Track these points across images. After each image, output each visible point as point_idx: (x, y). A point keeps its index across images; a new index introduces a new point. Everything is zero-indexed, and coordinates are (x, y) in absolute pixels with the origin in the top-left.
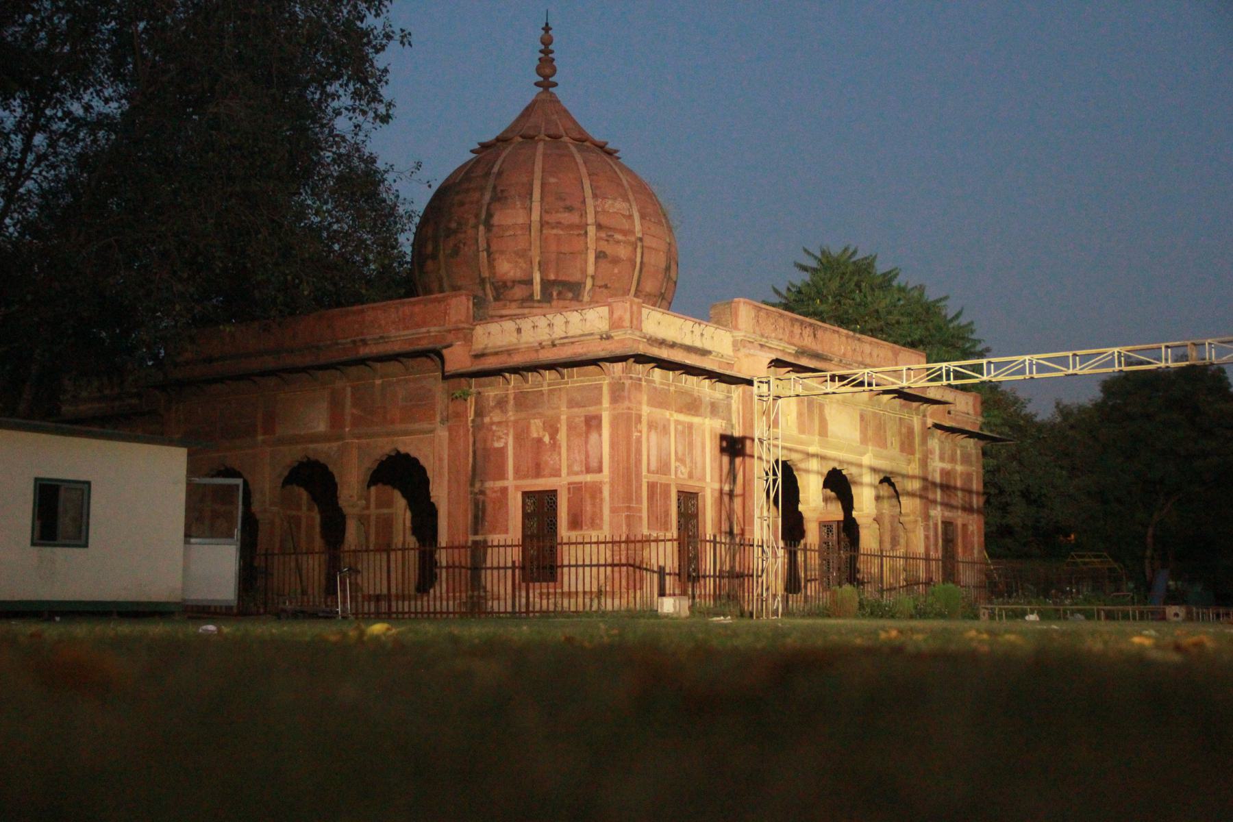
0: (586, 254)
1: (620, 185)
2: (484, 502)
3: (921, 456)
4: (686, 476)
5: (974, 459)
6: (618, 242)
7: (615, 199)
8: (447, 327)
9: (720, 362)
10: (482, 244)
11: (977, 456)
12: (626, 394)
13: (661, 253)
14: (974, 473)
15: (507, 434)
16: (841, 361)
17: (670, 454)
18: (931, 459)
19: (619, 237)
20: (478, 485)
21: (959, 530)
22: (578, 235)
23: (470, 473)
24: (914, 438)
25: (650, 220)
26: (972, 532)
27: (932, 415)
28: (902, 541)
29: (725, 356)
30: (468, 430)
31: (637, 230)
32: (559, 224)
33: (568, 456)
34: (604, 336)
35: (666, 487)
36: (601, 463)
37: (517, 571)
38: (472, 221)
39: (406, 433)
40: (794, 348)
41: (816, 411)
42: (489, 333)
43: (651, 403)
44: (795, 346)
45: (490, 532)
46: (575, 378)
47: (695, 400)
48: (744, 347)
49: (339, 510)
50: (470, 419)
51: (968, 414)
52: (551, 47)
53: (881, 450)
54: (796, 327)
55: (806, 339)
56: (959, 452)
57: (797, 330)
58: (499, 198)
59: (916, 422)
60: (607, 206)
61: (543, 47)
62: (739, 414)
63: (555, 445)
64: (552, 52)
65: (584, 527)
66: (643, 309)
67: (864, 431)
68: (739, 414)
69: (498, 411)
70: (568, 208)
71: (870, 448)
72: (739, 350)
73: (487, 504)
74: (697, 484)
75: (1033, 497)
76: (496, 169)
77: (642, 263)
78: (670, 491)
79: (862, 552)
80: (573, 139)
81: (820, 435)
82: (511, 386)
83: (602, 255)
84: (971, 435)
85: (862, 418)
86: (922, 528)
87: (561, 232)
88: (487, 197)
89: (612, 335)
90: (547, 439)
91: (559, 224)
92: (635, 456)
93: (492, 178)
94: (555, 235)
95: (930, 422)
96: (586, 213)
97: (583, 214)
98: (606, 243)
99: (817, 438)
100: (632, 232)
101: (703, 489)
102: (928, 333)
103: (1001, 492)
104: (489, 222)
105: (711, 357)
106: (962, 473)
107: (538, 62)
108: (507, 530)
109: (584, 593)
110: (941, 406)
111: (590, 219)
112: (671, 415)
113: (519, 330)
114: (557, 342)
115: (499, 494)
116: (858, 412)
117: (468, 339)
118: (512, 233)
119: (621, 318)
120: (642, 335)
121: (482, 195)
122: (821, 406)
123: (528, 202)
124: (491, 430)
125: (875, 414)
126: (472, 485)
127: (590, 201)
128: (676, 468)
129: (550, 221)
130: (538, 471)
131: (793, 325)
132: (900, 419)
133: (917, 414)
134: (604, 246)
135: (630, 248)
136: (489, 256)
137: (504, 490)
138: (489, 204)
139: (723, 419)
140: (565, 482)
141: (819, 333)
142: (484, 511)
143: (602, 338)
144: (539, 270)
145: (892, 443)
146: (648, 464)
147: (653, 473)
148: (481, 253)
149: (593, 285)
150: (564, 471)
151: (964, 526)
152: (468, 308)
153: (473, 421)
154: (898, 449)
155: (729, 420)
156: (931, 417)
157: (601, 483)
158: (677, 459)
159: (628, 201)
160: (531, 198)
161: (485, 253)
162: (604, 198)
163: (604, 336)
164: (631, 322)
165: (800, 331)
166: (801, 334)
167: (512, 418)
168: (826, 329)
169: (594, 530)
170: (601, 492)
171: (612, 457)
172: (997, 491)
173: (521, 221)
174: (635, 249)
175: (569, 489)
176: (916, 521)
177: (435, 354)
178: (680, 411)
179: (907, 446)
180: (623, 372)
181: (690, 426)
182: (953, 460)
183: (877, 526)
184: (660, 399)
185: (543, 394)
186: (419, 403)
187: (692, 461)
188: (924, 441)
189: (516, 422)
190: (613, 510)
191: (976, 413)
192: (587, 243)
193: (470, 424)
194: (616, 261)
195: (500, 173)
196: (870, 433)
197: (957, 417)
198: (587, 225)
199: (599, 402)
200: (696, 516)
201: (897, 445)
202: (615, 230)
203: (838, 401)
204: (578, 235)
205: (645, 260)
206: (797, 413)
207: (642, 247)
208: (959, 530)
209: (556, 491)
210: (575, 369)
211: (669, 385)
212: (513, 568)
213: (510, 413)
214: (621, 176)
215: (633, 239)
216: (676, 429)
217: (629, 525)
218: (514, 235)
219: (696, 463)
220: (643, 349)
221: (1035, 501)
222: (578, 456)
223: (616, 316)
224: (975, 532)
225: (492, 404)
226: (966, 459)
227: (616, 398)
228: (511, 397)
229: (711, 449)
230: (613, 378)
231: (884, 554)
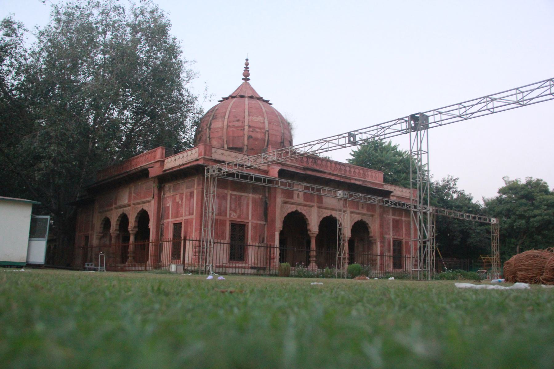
0: (244, 137)
4: (236, 217)
6: (257, 132)
17: (226, 208)
19: (257, 130)
22: (241, 130)
52: (248, 66)
55: (310, 163)
60: (253, 119)
61: (245, 66)
63: (182, 204)
64: (248, 68)
79: (312, 249)
87: (234, 129)
90: (180, 202)
98: (252, 133)
99: (315, 204)
106: (405, 221)
107: (243, 71)
118: (217, 130)
121: (210, 118)
123: (223, 119)
128: (230, 213)
130: (177, 216)
135: (263, 134)
136: (210, 139)
137: (168, 223)
138: (211, 121)
142: (163, 231)
144: (227, 144)
149: (247, 149)
150: (184, 215)
151: (407, 243)
162: (252, 116)
167: (172, 195)
173: (220, 126)
174: (265, 134)
181: (240, 197)
192: (244, 133)
198: (244, 126)
207: (269, 134)
215: (264, 131)
231: (407, 256)
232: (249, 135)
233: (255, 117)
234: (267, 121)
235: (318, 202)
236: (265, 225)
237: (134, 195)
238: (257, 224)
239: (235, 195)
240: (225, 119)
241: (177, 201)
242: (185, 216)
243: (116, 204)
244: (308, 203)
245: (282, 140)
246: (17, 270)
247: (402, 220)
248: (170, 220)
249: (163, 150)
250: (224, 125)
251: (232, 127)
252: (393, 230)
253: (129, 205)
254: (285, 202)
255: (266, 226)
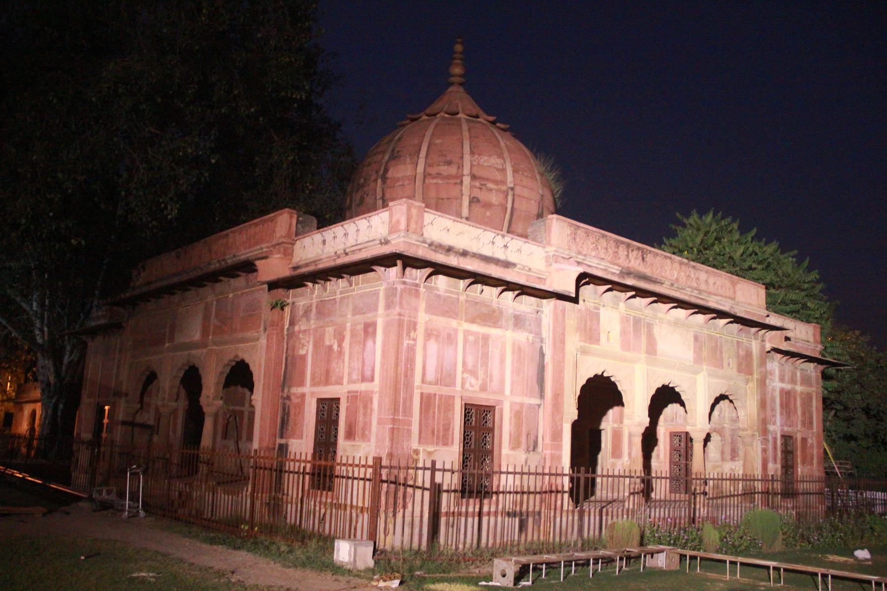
0: (461, 199)
1: (498, 145)
2: (289, 407)
3: (759, 377)
4: (477, 388)
5: (814, 380)
6: (491, 190)
7: (490, 156)
8: (274, 242)
9: (528, 275)
10: (379, 195)
11: (817, 379)
12: (397, 299)
13: (533, 202)
14: (814, 394)
15: (308, 342)
16: (672, 285)
17: (455, 364)
18: (771, 379)
19: (490, 185)
20: (286, 390)
21: (799, 442)
22: (456, 183)
23: (282, 378)
24: (752, 359)
25: (523, 174)
26: (812, 446)
27: (772, 340)
28: (741, 453)
29: (532, 270)
30: (284, 339)
31: (508, 180)
32: (439, 175)
33: (349, 363)
34: (383, 241)
35: (448, 402)
36: (373, 370)
37: (307, 477)
38: (373, 177)
39: (244, 340)
40: (617, 267)
41: (644, 331)
42: (304, 247)
43: (430, 310)
44: (619, 266)
45: (290, 438)
46: (360, 286)
47: (494, 311)
48: (556, 262)
49: (201, 408)
50: (286, 327)
51: (808, 342)
53: (717, 370)
54: (621, 249)
55: (633, 261)
56: (798, 374)
57: (622, 251)
58: (395, 157)
59: (755, 347)
60: (482, 160)
62: (549, 328)
63: (341, 353)
65: (357, 438)
66: (426, 215)
67: (698, 350)
68: (549, 328)
69: (304, 320)
70: (447, 162)
71: (705, 367)
72: (551, 265)
73: (291, 409)
74: (492, 397)
75: (872, 413)
76: (397, 138)
77: (512, 208)
78: (454, 404)
80: (469, 116)
81: (648, 352)
82: (314, 296)
83: (475, 200)
84: (810, 359)
85: (696, 338)
86: (759, 442)
87: (440, 182)
88: (387, 157)
89: (389, 239)
90: (335, 347)
91: (439, 175)
92: (406, 365)
93: (393, 144)
94: (435, 184)
95: (768, 347)
96: (463, 166)
97: (460, 167)
98: (479, 190)
99: (643, 356)
100: (504, 182)
101: (500, 402)
102: (778, 279)
103: (846, 409)
104: (385, 175)
105: (516, 269)
106: (802, 393)
108: (302, 435)
109: (352, 506)
110: (779, 332)
111: (466, 171)
112: (459, 324)
113: (324, 242)
114: (347, 251)
115: (299, 400)
116: (692, 334)
117: (288, 253)
118: (401, 183)
119: (398, 222)
120: (421, 239)
122: (650, 327)
123: (416, 158)
124: (299, 338)
125: (710, 337)
126: (283, 390)
127: (467, 157)
129: (431, 173)
130: (327, 382)
131: (618, 247)
132: (738, 342)
133: (755, 339)
134: (477, 193)
135: (502, 196)
137: (303, 396)
138: (387, 162)
139: (531, 332)
140: (346, 391)
141: (649, 258)
142: (288, 413)
143: (381, 243)
145: (729, 364)
146: (424, 375)
147: (430, 383)
148: (378, 201)
150: (345, 380)
151: (804, 440)
152: (290, 225)
153: (288, 329)
154: (735, 370)
155: (538, 334)
156: (769, 342)
157: (372, 392)
158: (465, 369)
159: (503, 158)
160: (418, 156)
161: (381, 202)
162: (480, 155)
163: (383, 241)
164: (408, 225)
165: (626, 253)
166: (627, 256)
167: (313, 326)
168: (657, 254)
169: (363, 441)
170: (372, 402)
171: (383, 365)
172: (842, 408)
175: (348, 397)
176: (753, 435)
177: (248, 267)
178: (473, 321)
179: (745, 365)
180: (397, 278)
181: (486, 338)
182: (793, 381)
183: (720, 438)
184: (445, 307)
185: (336, 302)
186: (252, 313)
187: (486, 372)
188: (763, 363)
189: (316, 330)
190: (380, 422)
191: (816, 342)
192: (461, 191)
193: (285, 333)
194: (488, 205)
195: (400, 139)
196: (705, 353)
197: (798, 344)
199: (376, 309)
200: (492, 430)
201: (733, 363)
202: (487, 179)
203: (669, 321)
204: (456, 183)
205: (516, 206)
206: (621, 331)
207: (514, 195)
208: (799, 442)
209: (339, 399)
210: (361, 276)
211: (458, 294)
212: (304, 473)
213: (312, 322)
214: (499, 138)
215: (504, 188)
216: (465, 340)
217: (392, 440)
218: (403, 185)
219: (491, 376)
220: (422, 252)
221: (875, 416)
222: (357, 365)
223: (394, 220)
224: (815, 445)
225: (301, 313)
226: (806, 381)
227: (389, 306)
228: (314, 306)
229: (513, 361)
230: (388, 283)
232: (472, 196)
233: (486, 158)
234: (511, 168)
235: (403, 321)
236: (539, 406)
237: (216, 321)
238: (522, 405)
239: (474, 334)
240: (418, 158)
241: (327, 343)
242: (351, 381)
243: (172, 339)
244: (627, 354)
245: (540, 211)
246: (98, 323)
247: (795, 392)
248: (307, 389)
249: (291, 217)
250: (418, 172)
251: (436, 178)
252: (781, 414)
253: (205, 346)
254: (584, 351)
255: (542, 407)
